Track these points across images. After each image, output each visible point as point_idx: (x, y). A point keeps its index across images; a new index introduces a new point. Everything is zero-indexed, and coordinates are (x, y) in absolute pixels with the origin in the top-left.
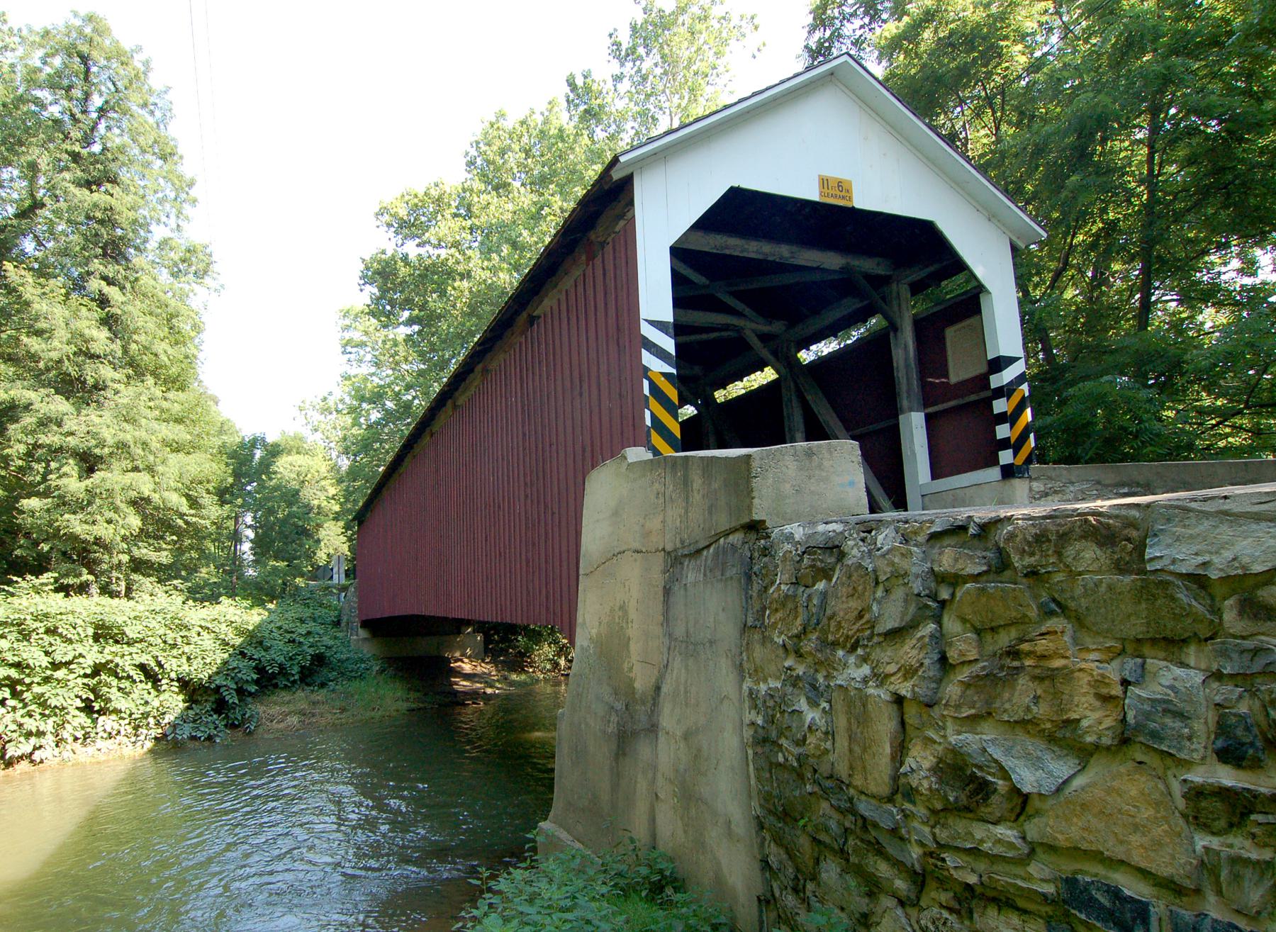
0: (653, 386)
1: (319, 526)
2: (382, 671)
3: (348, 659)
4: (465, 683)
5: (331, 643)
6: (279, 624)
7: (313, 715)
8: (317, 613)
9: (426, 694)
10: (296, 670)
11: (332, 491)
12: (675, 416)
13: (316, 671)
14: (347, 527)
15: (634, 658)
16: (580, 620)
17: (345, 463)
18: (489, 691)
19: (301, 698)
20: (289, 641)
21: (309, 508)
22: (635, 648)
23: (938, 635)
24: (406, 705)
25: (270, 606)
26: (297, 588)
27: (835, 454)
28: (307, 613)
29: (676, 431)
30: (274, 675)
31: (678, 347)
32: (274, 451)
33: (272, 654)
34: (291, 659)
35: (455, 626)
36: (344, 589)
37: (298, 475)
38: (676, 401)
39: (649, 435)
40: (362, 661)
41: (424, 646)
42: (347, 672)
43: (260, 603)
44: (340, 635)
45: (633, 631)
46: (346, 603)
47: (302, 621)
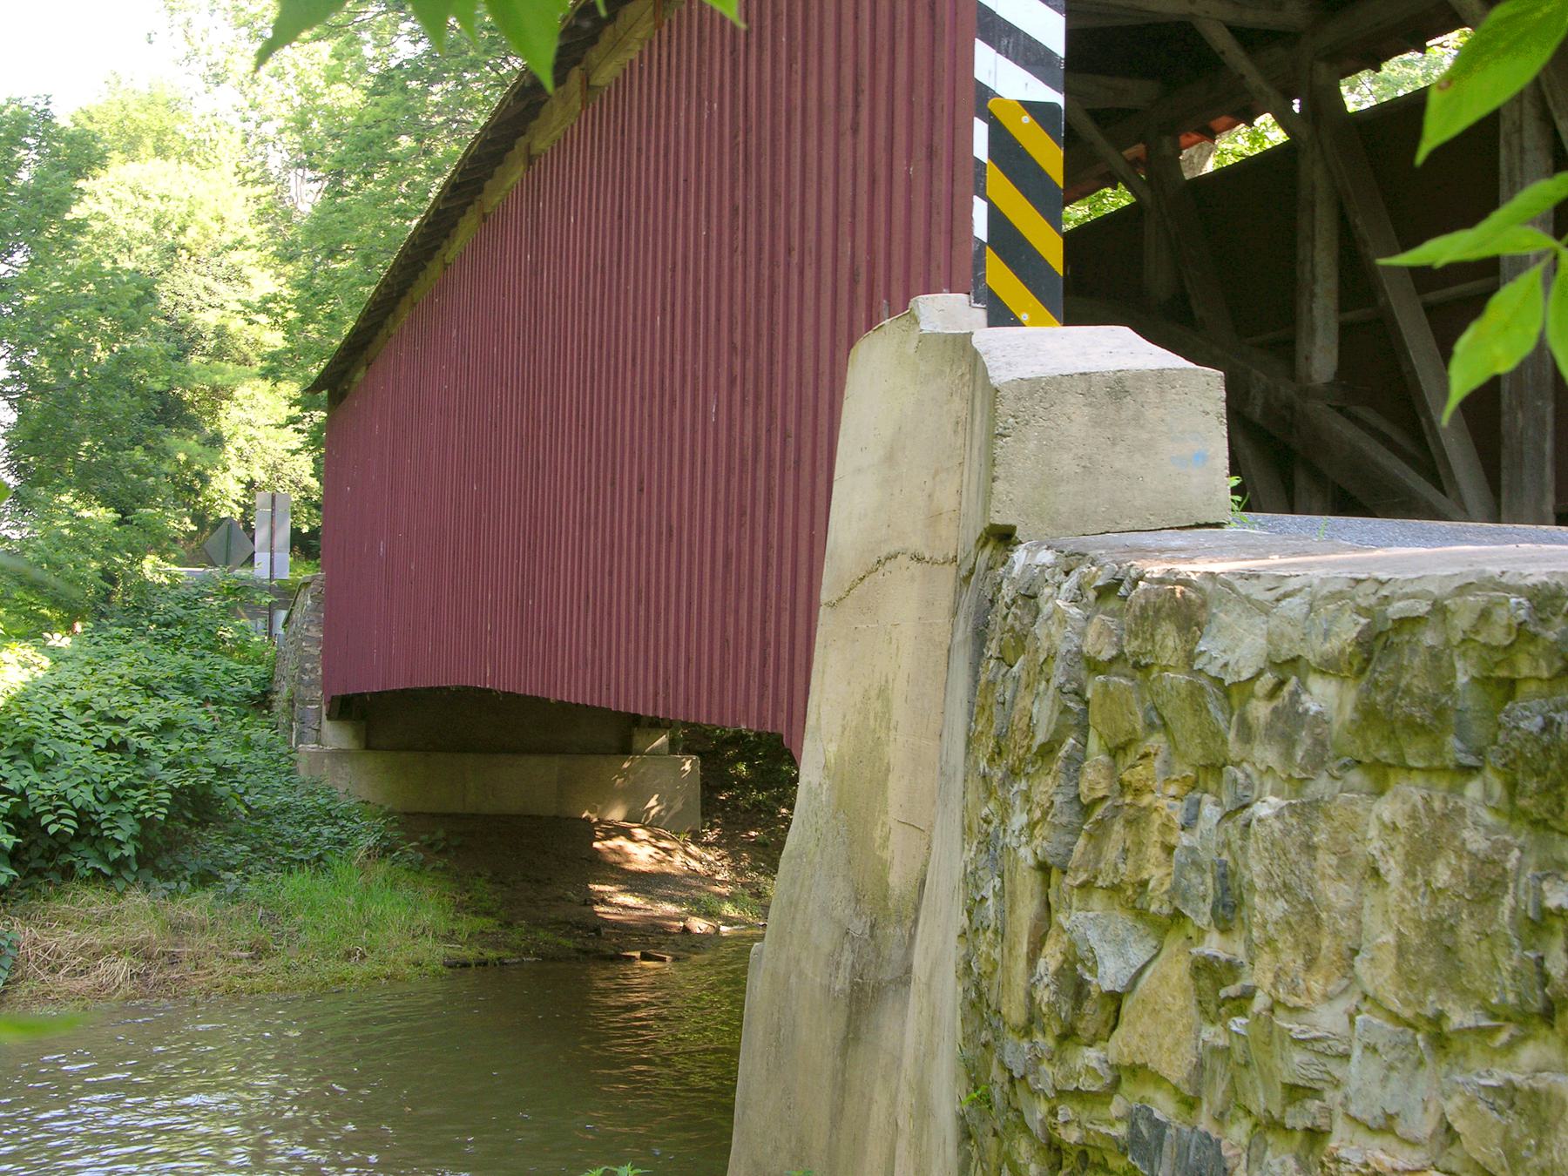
0: (1001, 140)
1: (220, 393)
2: (384, 850)
3: (284, 810)
4: (629, 900)
5: (233, 758)
6: (82, 694)
7: (174, 960)
8: (199, 669)
9: (508, 924)
10: (126, 829)
11: (265, 283)
12: (1055, 221)
13: (181, 835)
14: (307, 401)
15: (894, 814)
16: (811, 721)
17: (307, 195)
18: (699, 925)
19: (139, 912)
20: (110, 747)
21: (183, 340)
22: (896, 789)
23: (1078, 756)
24: (442, 950)
25: (60, 640)
26: (145, 588)
27: (1171, 395)
28: (172, 663)
29: (1052, 250)
30: (61, 844)
31: (1073, 37)
32: (79, 156)
33: (58, 781)
34: (113, 797)
35: (621, 732)
36: (286, 595)
37: (158, 225)
38: (1057, 175)
39: (979, 263)
40: (330, 818)
41: (520, 784)
42: (284, 844)
43: (33, 630)
44: (260, 734)
45: (896, 752)
46: (288, 644)
47: (150, 690)
